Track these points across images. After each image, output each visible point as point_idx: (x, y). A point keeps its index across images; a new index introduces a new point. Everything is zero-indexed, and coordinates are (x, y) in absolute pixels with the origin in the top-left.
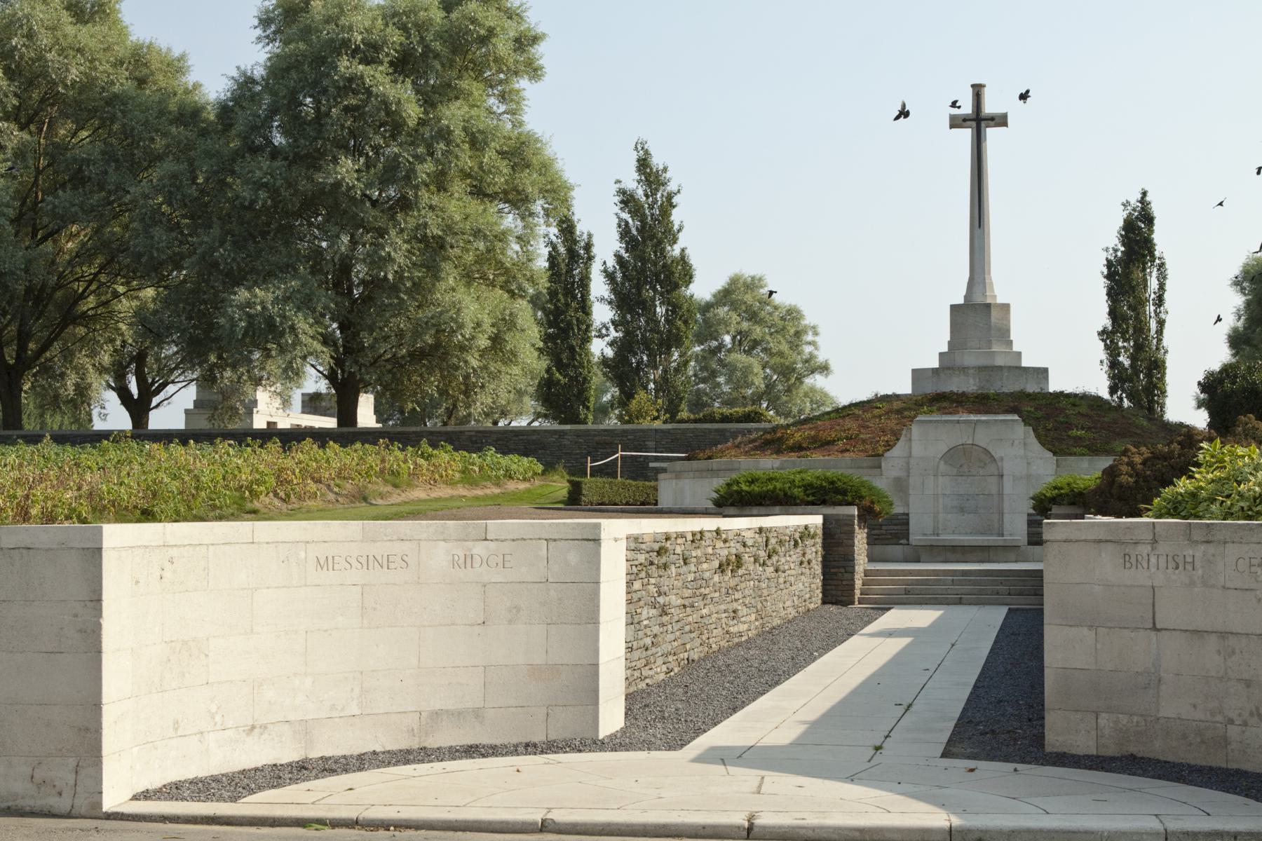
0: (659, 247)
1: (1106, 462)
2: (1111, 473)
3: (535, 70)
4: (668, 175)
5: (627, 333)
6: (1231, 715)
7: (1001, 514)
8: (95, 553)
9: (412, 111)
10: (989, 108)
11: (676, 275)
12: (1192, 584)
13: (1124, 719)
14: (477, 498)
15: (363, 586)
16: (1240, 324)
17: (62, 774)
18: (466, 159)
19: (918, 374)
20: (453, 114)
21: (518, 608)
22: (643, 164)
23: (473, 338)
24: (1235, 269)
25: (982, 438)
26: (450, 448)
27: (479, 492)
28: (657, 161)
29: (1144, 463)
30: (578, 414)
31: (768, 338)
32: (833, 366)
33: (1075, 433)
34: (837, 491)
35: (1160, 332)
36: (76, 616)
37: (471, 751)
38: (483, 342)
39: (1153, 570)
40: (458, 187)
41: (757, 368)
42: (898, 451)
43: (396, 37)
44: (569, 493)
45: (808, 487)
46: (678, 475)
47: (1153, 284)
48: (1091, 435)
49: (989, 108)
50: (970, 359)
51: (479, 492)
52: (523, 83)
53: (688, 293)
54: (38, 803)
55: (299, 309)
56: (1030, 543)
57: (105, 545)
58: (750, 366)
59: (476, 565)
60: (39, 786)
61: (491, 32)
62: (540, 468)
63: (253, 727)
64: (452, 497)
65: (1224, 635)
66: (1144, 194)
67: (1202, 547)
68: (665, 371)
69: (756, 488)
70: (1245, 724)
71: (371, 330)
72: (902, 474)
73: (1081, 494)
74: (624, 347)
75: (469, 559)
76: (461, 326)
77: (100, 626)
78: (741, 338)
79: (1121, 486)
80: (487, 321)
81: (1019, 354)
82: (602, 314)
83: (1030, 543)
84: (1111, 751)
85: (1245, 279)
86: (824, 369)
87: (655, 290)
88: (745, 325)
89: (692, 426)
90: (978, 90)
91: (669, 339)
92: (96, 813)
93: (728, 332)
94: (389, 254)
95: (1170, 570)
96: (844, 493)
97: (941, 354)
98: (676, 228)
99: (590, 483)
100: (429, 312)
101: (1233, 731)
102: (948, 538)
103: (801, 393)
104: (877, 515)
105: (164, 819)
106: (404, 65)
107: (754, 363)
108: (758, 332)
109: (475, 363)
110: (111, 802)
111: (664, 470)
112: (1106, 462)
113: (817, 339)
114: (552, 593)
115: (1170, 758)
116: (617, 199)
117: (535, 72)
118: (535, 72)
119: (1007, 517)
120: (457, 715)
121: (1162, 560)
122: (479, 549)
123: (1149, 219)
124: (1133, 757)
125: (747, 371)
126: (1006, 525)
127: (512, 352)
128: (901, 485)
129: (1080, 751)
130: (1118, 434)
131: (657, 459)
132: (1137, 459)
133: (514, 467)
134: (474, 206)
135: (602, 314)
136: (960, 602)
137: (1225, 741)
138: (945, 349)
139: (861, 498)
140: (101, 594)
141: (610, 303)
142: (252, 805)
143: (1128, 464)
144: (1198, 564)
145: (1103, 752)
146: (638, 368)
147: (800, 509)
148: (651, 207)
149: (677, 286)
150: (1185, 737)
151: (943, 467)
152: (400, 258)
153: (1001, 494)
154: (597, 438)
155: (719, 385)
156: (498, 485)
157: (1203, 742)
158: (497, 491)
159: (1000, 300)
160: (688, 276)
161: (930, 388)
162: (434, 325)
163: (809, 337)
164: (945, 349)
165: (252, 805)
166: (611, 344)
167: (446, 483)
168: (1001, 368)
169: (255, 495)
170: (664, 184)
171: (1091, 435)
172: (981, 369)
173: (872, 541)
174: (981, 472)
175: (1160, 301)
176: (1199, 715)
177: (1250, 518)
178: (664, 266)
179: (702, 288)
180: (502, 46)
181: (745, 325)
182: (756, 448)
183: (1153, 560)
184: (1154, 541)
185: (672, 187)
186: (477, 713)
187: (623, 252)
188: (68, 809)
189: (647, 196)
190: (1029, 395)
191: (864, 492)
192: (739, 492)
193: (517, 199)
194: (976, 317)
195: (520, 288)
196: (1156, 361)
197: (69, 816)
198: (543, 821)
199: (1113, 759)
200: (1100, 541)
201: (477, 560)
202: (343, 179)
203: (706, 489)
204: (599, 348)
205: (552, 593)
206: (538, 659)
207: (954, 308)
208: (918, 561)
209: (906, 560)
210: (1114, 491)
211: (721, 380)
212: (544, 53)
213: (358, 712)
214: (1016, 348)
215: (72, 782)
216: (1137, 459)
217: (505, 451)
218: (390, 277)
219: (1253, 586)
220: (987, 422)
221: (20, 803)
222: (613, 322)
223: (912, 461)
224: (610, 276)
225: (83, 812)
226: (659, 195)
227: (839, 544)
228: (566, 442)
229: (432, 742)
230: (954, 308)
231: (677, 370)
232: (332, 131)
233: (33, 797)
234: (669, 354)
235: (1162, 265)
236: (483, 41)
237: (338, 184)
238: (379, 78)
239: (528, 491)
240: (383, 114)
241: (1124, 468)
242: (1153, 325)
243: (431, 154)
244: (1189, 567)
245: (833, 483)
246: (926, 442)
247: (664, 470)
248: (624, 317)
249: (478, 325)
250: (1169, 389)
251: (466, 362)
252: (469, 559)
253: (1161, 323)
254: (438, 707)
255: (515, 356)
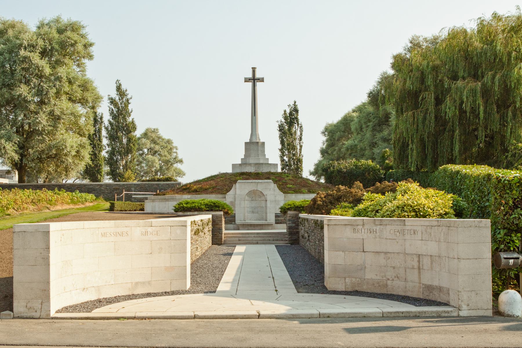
0: (124, 118)
1: (313, 196)
2: (314, 200)
3: (91, 56)
4: (127, 92)
5: (113, 148)
6: (388, 277)
7: (266, 213)
8: (47, 233)
9: (47, 71)
10: (258, 76)
11: (129, 128)
12: (376, 237)
13: (354, 280)
14: (78, 209)
15: (115, 242)
16: (324, 147)
17: (37, 305)
18: (66, 88)
19: (234, 166)
20: (62, 71)
21: (161, 248)
22: (119, 88)
23: (70, 151)
24: (322, 129)
25: (260, 188)
26: (65, 191)
27: (78, 207)
28: (123, 87)
29: (325, 197)
30: (97, 178)
31: (161, 150)
32: (184, 160)
33: (288, 186)
34: (216, 206)
35: (301, 150)
36: (41, 253)
37: (149, 295)
38: (74, 153)
39: (363, 233)
40: (64, 97)
41: (157, 161)
42: (231, 192)
43: (41, 42)
44: (110, 207)
45: (206, 205)
46: (153, 201)
47: (298, 133)
48: (294, 186)
49: (258, 76)
50: (252, 161)
51: (78, 207)
52: (86, 61)
53: (135, 134)
54: (29, 315)
55: (6, 141)
56: (276, 223)
57: (51, 230)
58: (155, 160)
59: (149, 234)
60: (29, 309)
61: (76, 42)
62: (94, 198)
63: (84, 289)
64: (70, 209)
65: (386, 253)
66: (295, 102)
67: (379, 226)
68: (126, 162)
69: (189, 206)
70: (393, 280)
71: (33, 148)
72: (233, 200)
73: (297, 207)
74: (112, 153)
75: (146, 233)
76: (66, 147)
77: (49, 256)
78: (150, 149)
79: (318, 205)
80: (75, 145)
81: (268, 159)
82: (105, 141)
83: (276, 223)
84: (350, 289)
85: (326, 131)
86: (181, 161)
87: (123, 133)
88: (152, 146)
89: (147, 183)
90: (254, 70)
91: (127, 151)
92: (48, 317)
93: (146, 148)
94: (40, 121)
95: (368, 234)
96: (219, 207)
97: (242, 159)
98: (130, 111)
99: (117, 204)
100: (54, 142)
101: (389, 282)
102: (248, 222)
103: (172, 169)
104: (229, 214)
105: (71, 318)
106: (44, 54)
107: (156, 158)
108: (157, 148)
109: (70, 160)
110: (53, 314)
111: (146, 199)
112: (313, 196)
113: (177, 151)
114: (172, 243)
115: (369, 291)
116: (109, 101)
117: (91, 57)
118: (91, 57)
119: (268, 214)
120: (144, 283)
121: (366, 230)
122: (150, 229)
123: (297, 111)
124: (357, 291)
125: (153, 162)
126: (268, 218)
127: (82, 157)
128: (233, 203)
129: (340, 290)
130: (303, 186)
131: (135, 194)
132: (323, 196)
133: (88, 198)
134: (70, 104)
135: (105, 141)
136: (257, 243)
137: (387, 285)
138: (243, 157)
139: (224, 209)
140: (49, 246)
141: (106, 138)
142: (97, 312)
143: (320, 197)
144: (377, 232)
145: (347, 290)
146: (117, 161)
147: (204, 212)
148: (121, 104)
149: (131, 132)
150: (373, 284)
151: (247, 198)
152: (44, 122)
153: (266, 207)
154: (114, 187)
155: (143, 166)
156: (83, 204)
157: (379, 286)
158: (83, 206)
159: (262, 141)
160: (135, 128)
161: (238, 171)
162: (56, 147)
163: (175, 150)
164: (243, 157)
165: (97, 312)
166: (107, 152)
167: (66, 203)
168: (262, 164)
169: (8, 209)
170: (126, 96)
171: (294, 186)
172: (256, 164)
173: (226, 223)
174: (259, 199)
175: (301, 139)
176: (378, 278)
177: (390, 217)
178: (126, 125)
179: (138, 133)
180: (80, 47)
181: (152, 146)
182: (181, 191)
183: (363, 230)
184: (363, 225)
185: (129, 97)
186: (149, 283)
187: (111, 120)
188: (39, 316)
189: (120, 100)
190: (272, 173)
191: (225, 206)
192: (183, 207)
193: (83, 102)
194: (254, 146)
195: (84, 133)
196: (299, 160)
197: (39, 318)
198: (195, 315)
199: (351, 292)
200: (346, 225)
201: (149, 233)
202: (22, 93)
203: (170, 206)
204: (104, 154)
205: (172, 243)
206: (168, 265)
207: (246, 143)
208: (239, 229)
209: (234, 229)
210: (316, 206)
211: (144, 165)
212: (93, 50)
213: (113, 283)
214: (267, 157)
215: (40, 308)
216: (323, 196)
217: (81, 192)
218: (40, 129)
219: (396, 238)
220: (261, 182)
221: (22, 315)
222: (108, 145)
223: (236, 196)
224: (107, 129)
225: (44, 317)
226: (124, 99)
227: (217, 224)
228: (103, 188)
229: (136, 293)
230: (246, 143)
231: (131, 162)
232: (18, 76)
233: (27, 313)
234: (128, 156)
235: (301, 127)
236: (72, 45)
237: (20, 95)
238: (36, 58)
239: (94, 206)
240: (37, 71)
241: (319, 199)
242: (298, 147)
243: (54, 86)
244: (375, 233)
245: (214, 204)
246: (241, 189)
247: (146, 199)
248: (111, 143)
249: (72, 147)
250: (303, 169)
251: (67, 160)
252: (146, 233)
253: (301, 146)
254: (137, 281)
255: (84, 158)
